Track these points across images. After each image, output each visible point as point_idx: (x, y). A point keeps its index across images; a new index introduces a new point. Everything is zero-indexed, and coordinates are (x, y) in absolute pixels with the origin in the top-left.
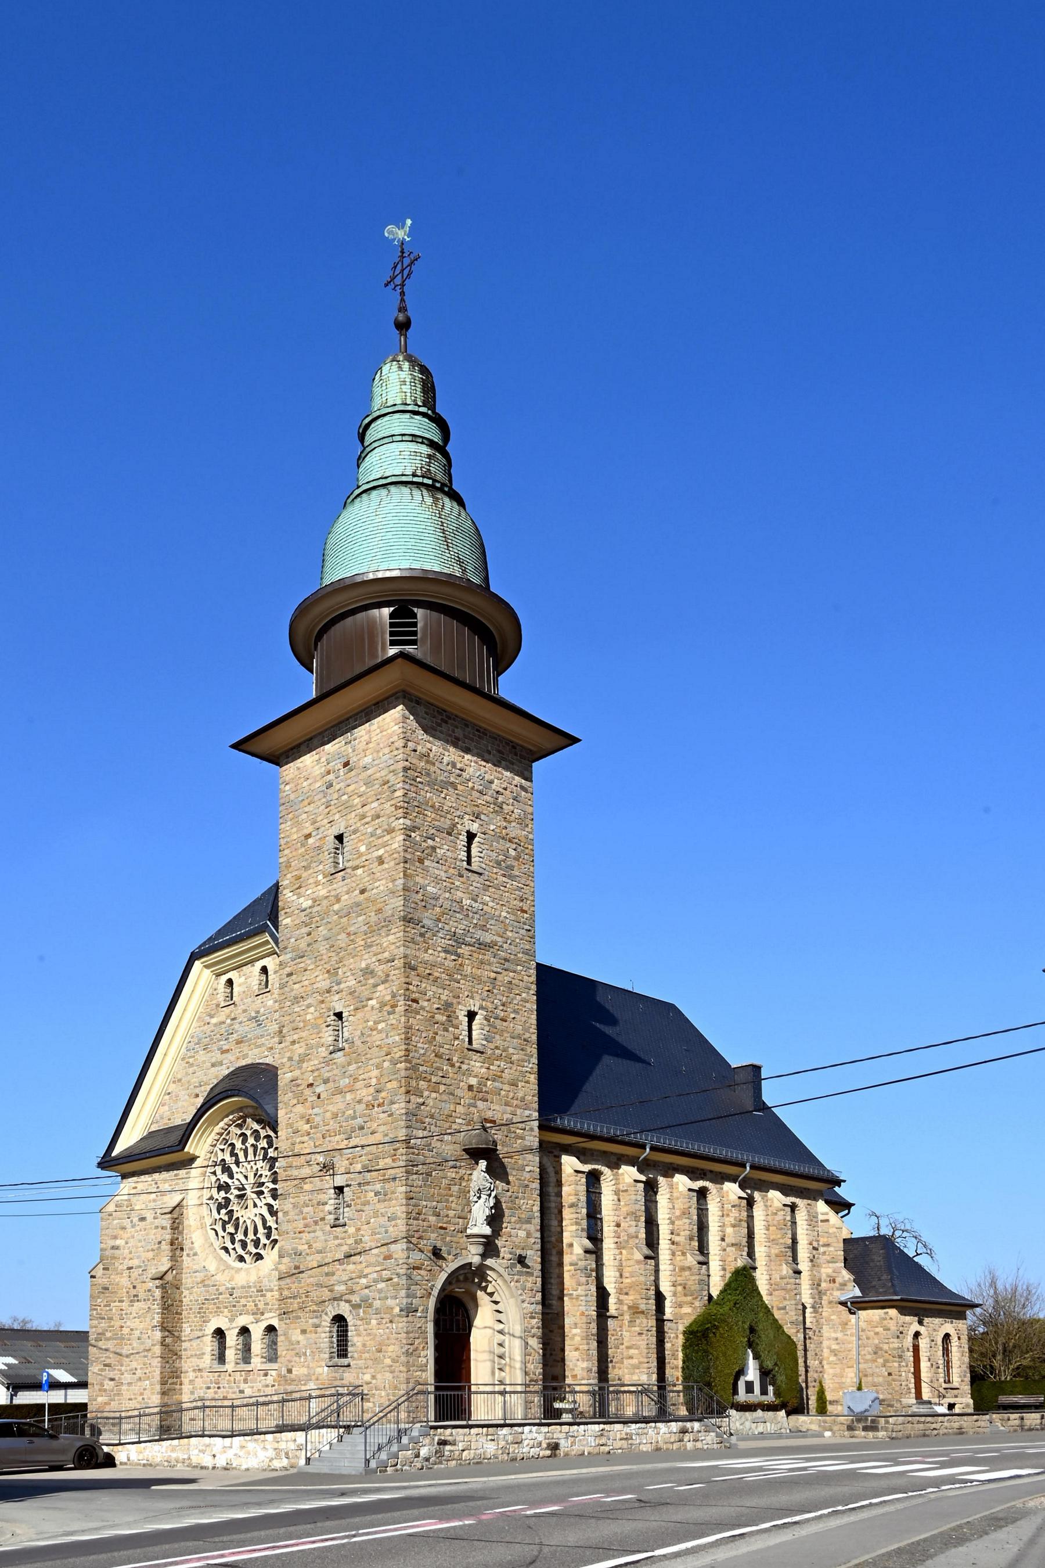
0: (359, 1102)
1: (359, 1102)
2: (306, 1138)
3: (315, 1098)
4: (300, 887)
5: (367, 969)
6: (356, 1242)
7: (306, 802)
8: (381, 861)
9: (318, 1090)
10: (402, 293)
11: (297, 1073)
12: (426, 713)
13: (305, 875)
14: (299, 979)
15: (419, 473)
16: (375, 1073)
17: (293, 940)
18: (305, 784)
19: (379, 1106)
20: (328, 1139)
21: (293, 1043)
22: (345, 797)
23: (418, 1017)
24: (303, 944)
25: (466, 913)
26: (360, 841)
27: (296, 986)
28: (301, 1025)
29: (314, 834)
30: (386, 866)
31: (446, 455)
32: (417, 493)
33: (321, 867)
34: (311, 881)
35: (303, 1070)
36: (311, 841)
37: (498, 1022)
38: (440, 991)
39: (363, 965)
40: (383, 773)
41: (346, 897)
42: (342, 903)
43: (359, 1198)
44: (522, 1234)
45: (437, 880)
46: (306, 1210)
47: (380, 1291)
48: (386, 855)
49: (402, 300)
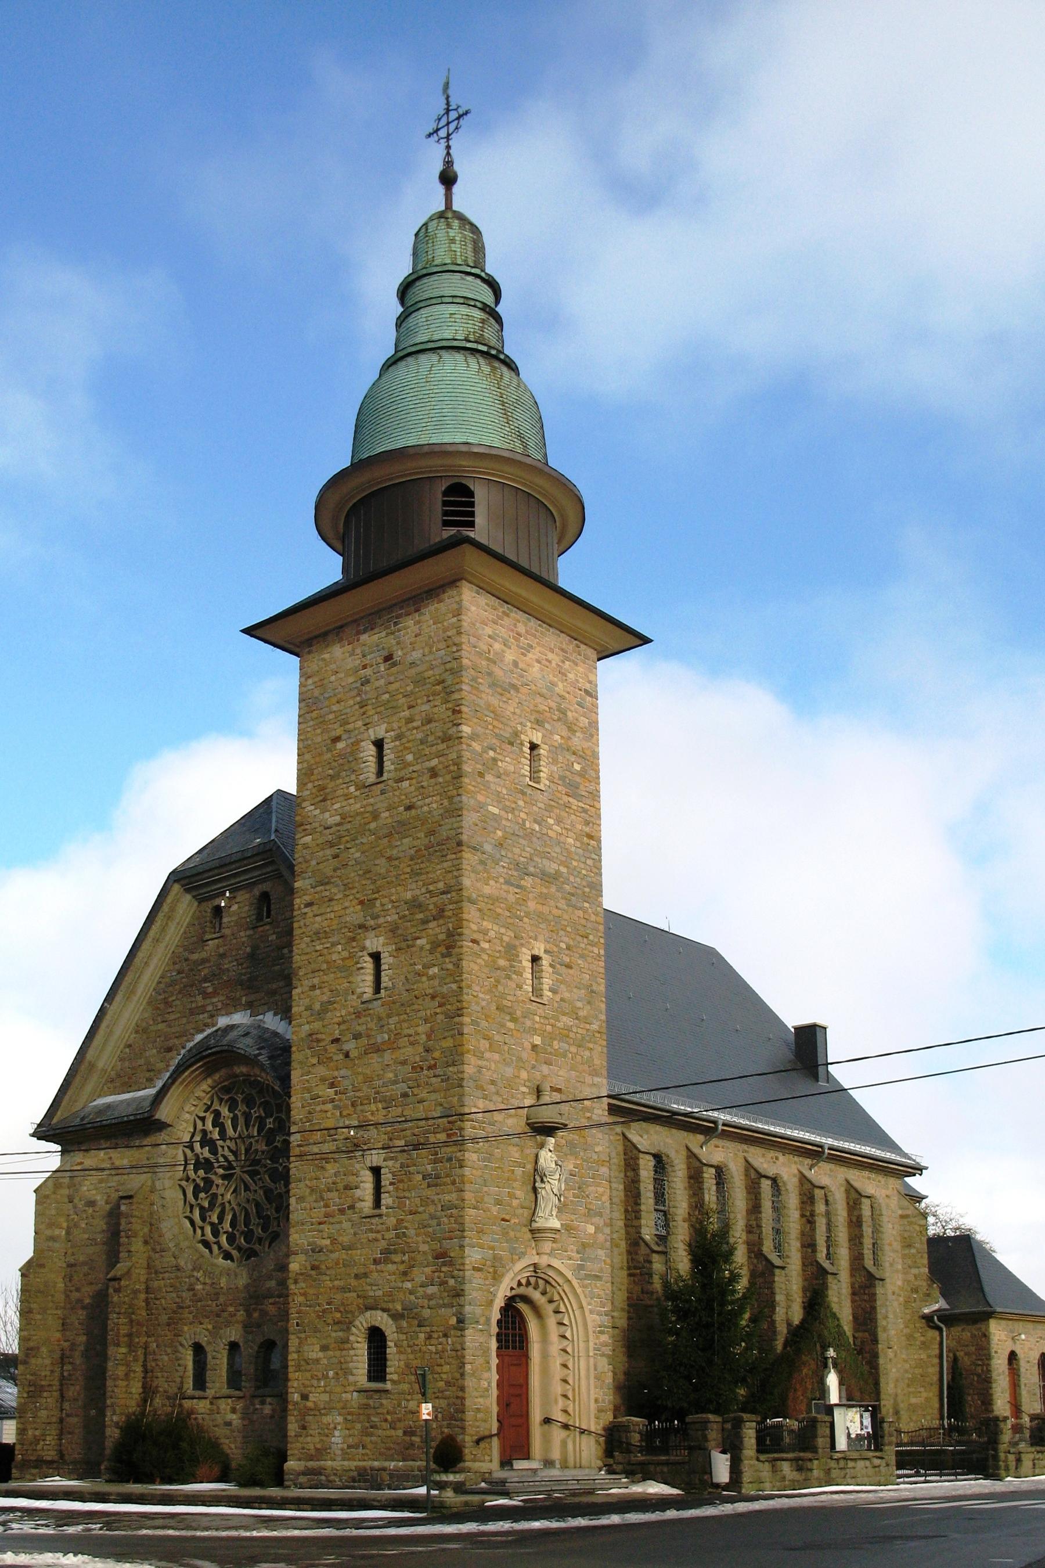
0: (404, 1063)
1: (404, 1063)
2: (329, 1106)
3: (341, 1056)
4: (324, 800)
5: (414, 901)
6: (397, 1236)
7: (334, 700)
8: (433, 773)
9: (346, 1047)
10: (448, 147)
11: (317, 1025)
12: (487, 604)
13: (331, 785)
14: (322, 910)
15: (471, 337)
16: (423, 1029)
17: (314, 863)
18: (333, 678)
19: (430, 1068)
20: (359, 1108)
21: (313, 988)
22: (387, 696)
23: (479, 961)
24: (327, 869)
25: (530, 835)
26: (406, 748)
27: (318, 919)
28: (325, 966)
29: (344, 737)
30: (441, 780)
31: (498, 319)
32: (473, 361)
33: (353, 777)
34: (340, 792)
35: (326, 1022)
36: (340, 745)
37: (563, 970)
38: (503, 930)
39: (409, 895)
40: (437, 671)
41: (387, 814)
42: (381, 822)
43: (402, 1181)
44: (591, 1229)
45: (499, 799)
46: (330, 1195)
47: (430, 1298)
48: (440, 766)
49: (448, 154)
